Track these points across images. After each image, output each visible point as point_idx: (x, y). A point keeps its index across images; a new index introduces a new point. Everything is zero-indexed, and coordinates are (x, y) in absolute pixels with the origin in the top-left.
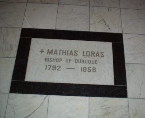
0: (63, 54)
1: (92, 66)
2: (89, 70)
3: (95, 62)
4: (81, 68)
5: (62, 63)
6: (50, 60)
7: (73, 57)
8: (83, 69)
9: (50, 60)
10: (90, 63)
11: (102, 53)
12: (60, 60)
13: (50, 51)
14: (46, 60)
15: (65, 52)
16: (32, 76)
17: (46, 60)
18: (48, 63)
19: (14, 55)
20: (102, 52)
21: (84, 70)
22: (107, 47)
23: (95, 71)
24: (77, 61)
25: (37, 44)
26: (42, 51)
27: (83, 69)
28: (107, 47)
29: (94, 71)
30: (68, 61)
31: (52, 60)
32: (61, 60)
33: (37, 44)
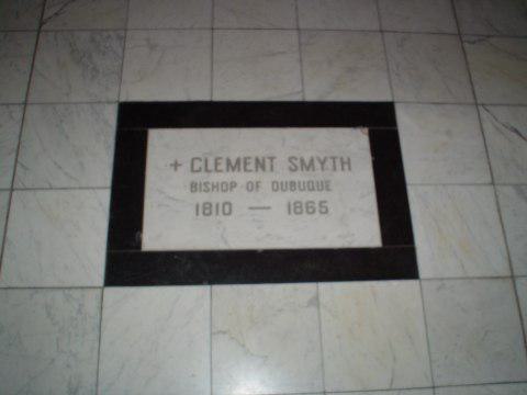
0: (343, 169)
1: (316, 197)
2: (324, 210)
3: (325, 186)
4: (197, 206)
5: (239, 198)
6: (203, 187)
7: (266, 178)
8: (292, 207)
9: (203, 187)
10: (313, 189)
11: (293, 167)
12: (232, 187)
13: (233, 162)
14: (194, 187)
15: (234, 166)
16: (161, 232)
17: (194, 187)
18: (201, 198)
19: (346, 163)
20: (293, 157)
21: (295, 208)
22: (355, 142)
23: (230, 213)
24: (277, 187)
25: (163, 144)
26: (176, 165)
27: (292, 207)
28: (355, 142)
29: (298, 210)
30: (253, 187)
31: (210, 186)
32: (233, 185)
33: (163, 144)
